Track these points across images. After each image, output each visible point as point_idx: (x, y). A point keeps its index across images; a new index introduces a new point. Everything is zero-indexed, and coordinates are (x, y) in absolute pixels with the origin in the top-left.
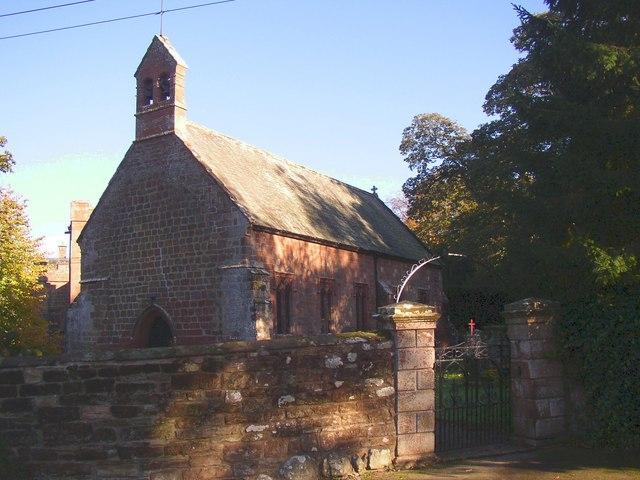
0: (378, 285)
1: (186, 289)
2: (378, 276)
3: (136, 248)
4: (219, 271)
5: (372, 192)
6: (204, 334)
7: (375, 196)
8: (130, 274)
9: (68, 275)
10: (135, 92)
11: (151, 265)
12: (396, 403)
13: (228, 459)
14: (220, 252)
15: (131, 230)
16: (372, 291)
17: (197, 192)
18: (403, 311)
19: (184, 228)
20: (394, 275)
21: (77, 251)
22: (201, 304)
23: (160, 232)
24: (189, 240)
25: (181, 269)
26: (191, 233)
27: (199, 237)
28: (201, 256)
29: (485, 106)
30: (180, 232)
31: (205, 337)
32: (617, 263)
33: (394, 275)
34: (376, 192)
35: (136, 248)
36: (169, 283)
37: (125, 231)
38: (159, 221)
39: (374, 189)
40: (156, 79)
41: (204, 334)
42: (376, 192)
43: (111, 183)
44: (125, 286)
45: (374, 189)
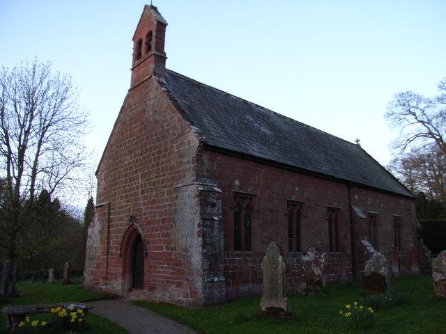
0: (351, 210)
2: (352, 202)
3: (126, 176)
4: (176, 190)
5: (356, 143)
6: (165, 250)
7: (358, 146)
9: (77, 193)
11: (133, 189)
12: (353, 252)
14: (178, 172)
16: (347, 215)
17: (165, 121)
18: (363, 216)
19: (154, 154)
20: (368, 203)
21: (95, 180)
22: (164, 221)
23: (140, 160)
26: (159, 158)
33: (368, 203)
34: (359, 142)
35: (126, 176)
36: (144, 204)
39: (358, 141)
40: (150, 38)
41: (165, 250)
42: (359, 142)
43: (115, 126)
45: (358, 141)
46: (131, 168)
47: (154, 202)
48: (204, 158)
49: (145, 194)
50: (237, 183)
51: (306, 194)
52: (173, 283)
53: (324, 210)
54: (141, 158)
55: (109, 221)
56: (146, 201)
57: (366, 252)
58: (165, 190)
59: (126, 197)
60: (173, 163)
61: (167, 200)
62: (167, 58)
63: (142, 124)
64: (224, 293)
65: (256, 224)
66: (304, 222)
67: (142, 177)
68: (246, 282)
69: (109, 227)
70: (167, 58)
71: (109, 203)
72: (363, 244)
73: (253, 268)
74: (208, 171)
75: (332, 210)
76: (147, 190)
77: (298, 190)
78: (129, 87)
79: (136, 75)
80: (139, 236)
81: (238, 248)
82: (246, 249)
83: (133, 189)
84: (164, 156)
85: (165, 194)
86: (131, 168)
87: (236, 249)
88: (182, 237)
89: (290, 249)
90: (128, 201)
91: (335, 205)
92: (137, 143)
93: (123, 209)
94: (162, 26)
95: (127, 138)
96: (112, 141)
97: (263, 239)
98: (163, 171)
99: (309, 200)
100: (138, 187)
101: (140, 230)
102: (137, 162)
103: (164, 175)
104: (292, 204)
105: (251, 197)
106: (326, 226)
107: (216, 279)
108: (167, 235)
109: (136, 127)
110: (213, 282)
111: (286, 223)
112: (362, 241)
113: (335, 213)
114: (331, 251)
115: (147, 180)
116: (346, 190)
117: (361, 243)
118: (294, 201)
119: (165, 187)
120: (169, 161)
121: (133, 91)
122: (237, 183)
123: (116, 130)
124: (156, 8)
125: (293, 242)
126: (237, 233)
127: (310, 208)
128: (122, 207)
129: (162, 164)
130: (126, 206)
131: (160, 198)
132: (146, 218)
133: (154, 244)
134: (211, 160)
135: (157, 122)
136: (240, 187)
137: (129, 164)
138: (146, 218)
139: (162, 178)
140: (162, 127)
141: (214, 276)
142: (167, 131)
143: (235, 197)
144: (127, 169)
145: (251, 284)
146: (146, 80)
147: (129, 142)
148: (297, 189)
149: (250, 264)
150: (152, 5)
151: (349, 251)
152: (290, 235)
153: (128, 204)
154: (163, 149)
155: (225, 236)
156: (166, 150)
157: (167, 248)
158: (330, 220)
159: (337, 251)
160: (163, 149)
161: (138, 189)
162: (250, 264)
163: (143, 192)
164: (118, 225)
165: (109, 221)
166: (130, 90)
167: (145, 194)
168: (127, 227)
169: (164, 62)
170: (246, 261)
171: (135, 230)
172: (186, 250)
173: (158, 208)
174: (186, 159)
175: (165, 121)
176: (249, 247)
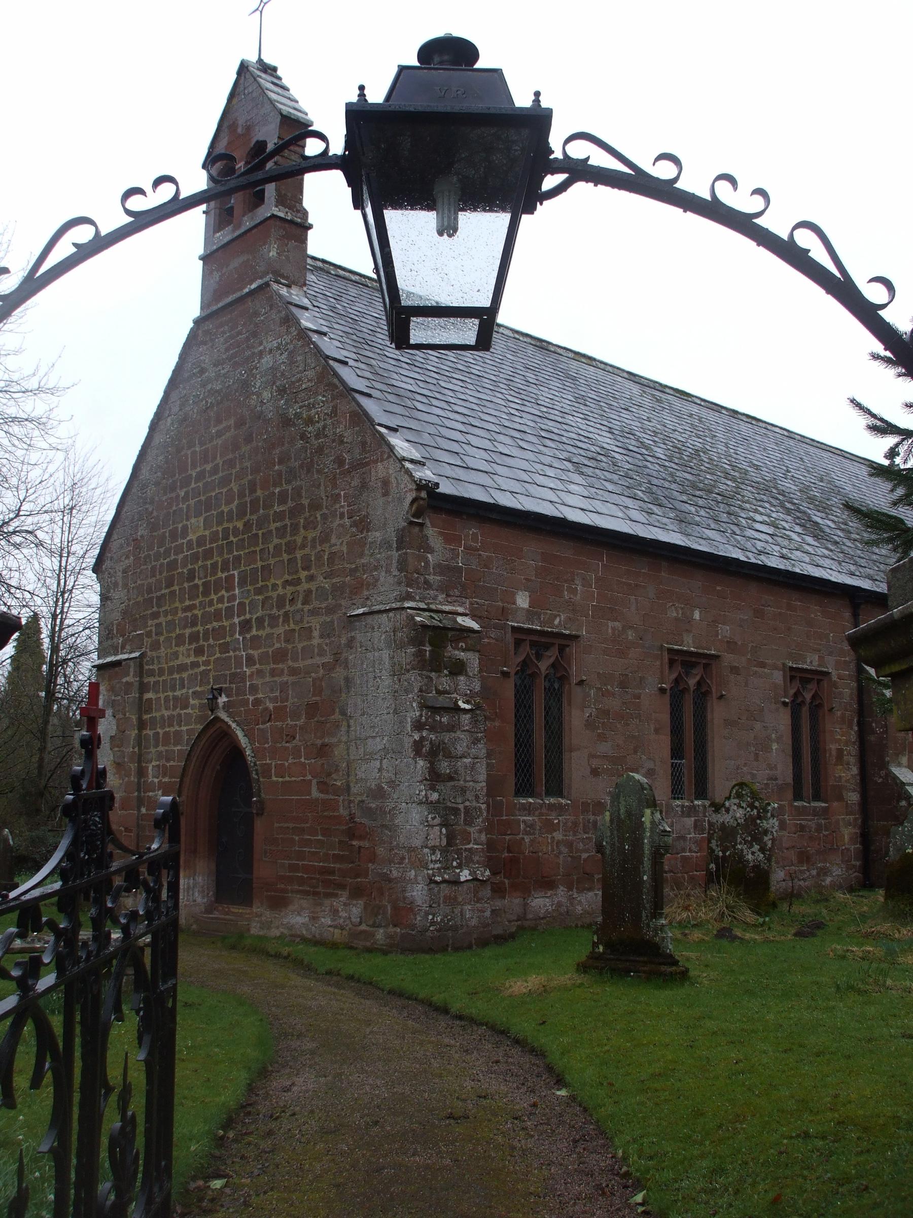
1: (281, 673)
3: (191, 576)
5: (886, 462)
6: (315, 793)
8: (180, 641)
10: (736, 208)
11: (217, 615)
13: (699, 824)
14: (353, 571)
15: (185, 530)
19: (279, 516)
24: (291, 548)
25: (274, 620)
26: (295, 528)
27: (311, 535)
28: (313, 586)
29: (450, 236)
30: (273, 526)
31: (317, 800)
32: (580, 908)
35: (191, 576)
36: (250, 660)
37: (174, 536)
38: (234, 506)
41: (315, 793)
44: (171, 671)
46: (208, 554)
47: (280, 656)
48: (431, 532)
49: (254, 632)
50: (523, 601)
51: (725, 630)
52: (342, 887)
53: (778, 677)
54: (240, 525)
55: (143, 707)
56: (255, 653)
57: (903, 803)
58: (315, 623)
59: (194, 637)
60: (339, 544)
61: (321, 653)
62: (310, 227)
63: (240, 423)
64: (488, 914)
65: (576, 719)
66: (717, 714)
67: (243, 582)
68: (548, 884)
69: (142, 725)
70: (310, 227)
71: (142, 656)
72: (895, 778)
73: (570, 845)
74: (441, 569)
75: (797, 676)
76: (260, 621)
77: (701, 620)
78: (196, 312)
79: (217, 276)
80: (236, 752)
81: (524, 788)
82: (549, 793)
83: (217, 615)
84: (310, 525)
85: (316, 634)
86: (208, 554)
87: (519, 792)
88: (368, 757)
89: (677, 791)
90: (199, 651)
91: (811, 662)
92: (225, 481)
93: (185, 675)
94: (356, 207)
95: (194, 466)
96: (145, 473)
97: (595, 763)
98: (306, 568)
99: (731, 645)
100: (230, 613)
101: (240, 734)
102: (226, 537)
103: (311, 578)
104: (683, 661)
105: (564, 642)
106: (782, 721)
107: (465, 875)
108: (323, 751)
109: (219, 434)
110: (456, 882)
111: (666, 718)
112: (896, 771)
113: (812, 686)
114: (798, 796)
115: (258, 591)
116: (847, 614)
117: (890, 774)
118: (691, 654)
119: (314, 612)
120: (325, 538)
121: (209, 325)
122: (523, 601)
123: (158, 439)
124: (275, 69)
125: (685, 771)
126: (523, 743)
127: (735, 670)
128: (182, 668)
129: (303, 546)
130: (195, 665)
131: (300, 646)
132: (257, 702)
133: (276, 768)
134: (449, 539)
135: (286, 422)
136: (530, 614)
137: (201, 541)
138: (257, 702)
139: (305, 586)
140: (303, 437)
141: (460, 866)
142: (320, 450)
143: (518, 643)
144: (195, 558)
145: (561, 890)
146: (252, 293)
147: (201, 476)
148: (697, 615)
149: (558, 836)
150: (260, 60)
151: (854, 797)
152: (677, 751)
153: (201, 659)
154: (306, 502)
155: (489, 755)
156: (315, 506)
157: (324, 786)
158: (795, 707)
159: (817, 797)
160: (306, 502)
161: (230, 616)
162: (558, 836)
163: (245, 626)
164: (170, 721)
165: (143, 707)
166: (198, 322)
167: (254, 632)
168: (200, 727)
169: (303, 241)
170: (550, 827)
171: (225, 734)
172: (379, 793)
173: (293, 672)
174: (376, 536)
175: (310, 421)
176: (556, 786)
